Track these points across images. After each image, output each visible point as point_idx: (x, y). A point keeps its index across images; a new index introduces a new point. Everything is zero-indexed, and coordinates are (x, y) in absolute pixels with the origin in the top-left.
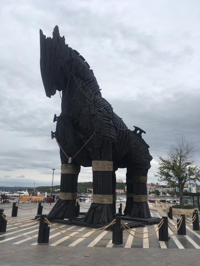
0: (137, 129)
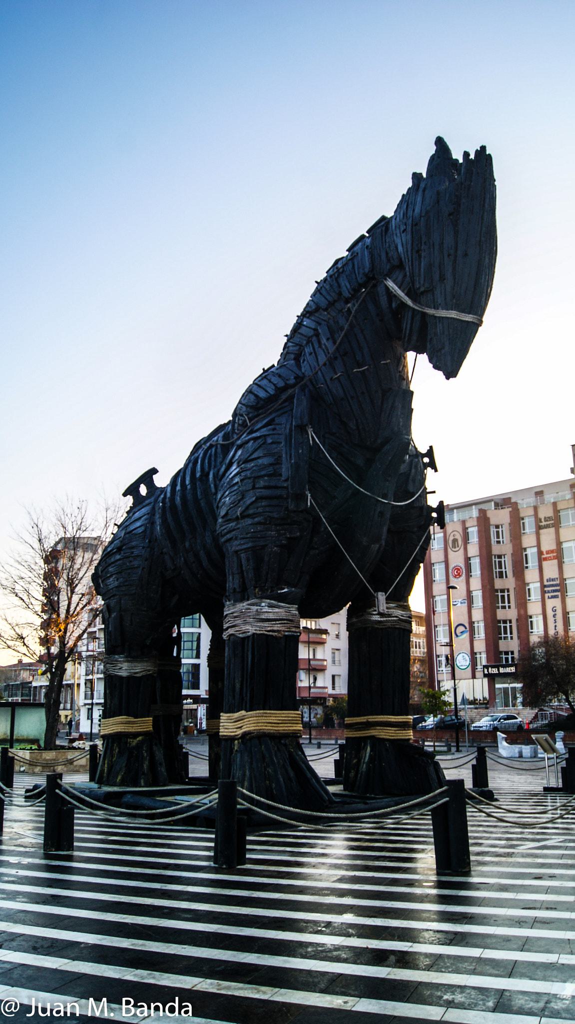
0: (132, 490)
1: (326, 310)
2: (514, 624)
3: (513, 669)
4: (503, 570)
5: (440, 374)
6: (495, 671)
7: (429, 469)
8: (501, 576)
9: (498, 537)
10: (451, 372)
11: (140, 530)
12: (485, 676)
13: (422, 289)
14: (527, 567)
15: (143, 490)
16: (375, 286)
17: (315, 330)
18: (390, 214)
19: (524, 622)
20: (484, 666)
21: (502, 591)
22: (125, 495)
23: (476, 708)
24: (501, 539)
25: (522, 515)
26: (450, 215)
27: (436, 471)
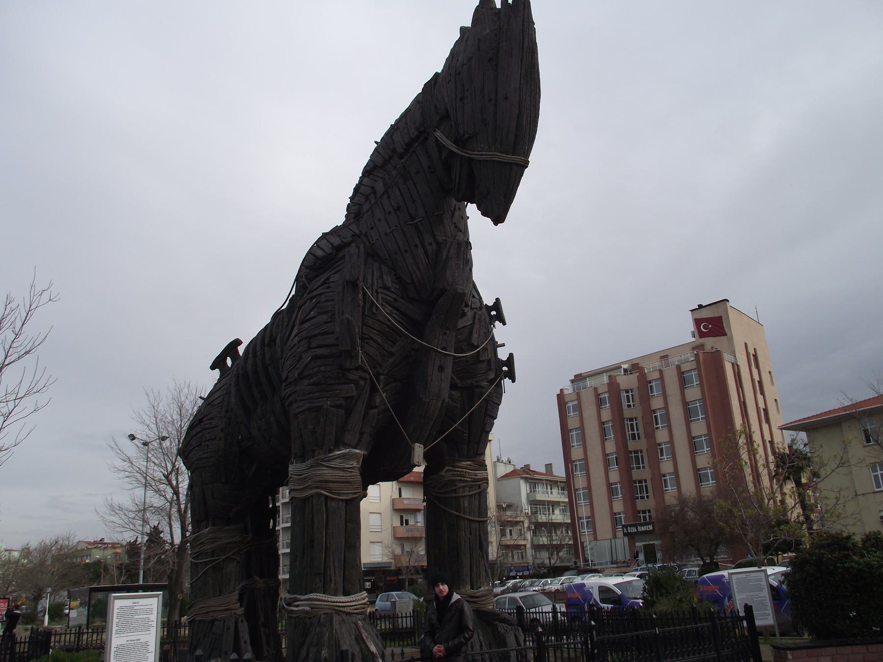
0: (218, 363)
1: (382, 167)
2: (649, 484)
3: (650, 527)
4: (636, 432)
5: (488, 221)
6: (634, 530)
7: (497, 323)
8: (633, 437)
9: (628, 401)
10: (498, 217)
11: (218, 401)
12: (625, 534)
13: (466, 136)
14: (657, 428)
15: (229, 362)
16: (426, 139)
17: (373, 188)
18: (440, 71)
19: (659, 479)
20: (623, 526)
21: (636, 452)
22: (213, 367)
23: (618, 567)
24: (631, 403)
25: (649, 379)
26: (489, 60)
27: (504, 324)
